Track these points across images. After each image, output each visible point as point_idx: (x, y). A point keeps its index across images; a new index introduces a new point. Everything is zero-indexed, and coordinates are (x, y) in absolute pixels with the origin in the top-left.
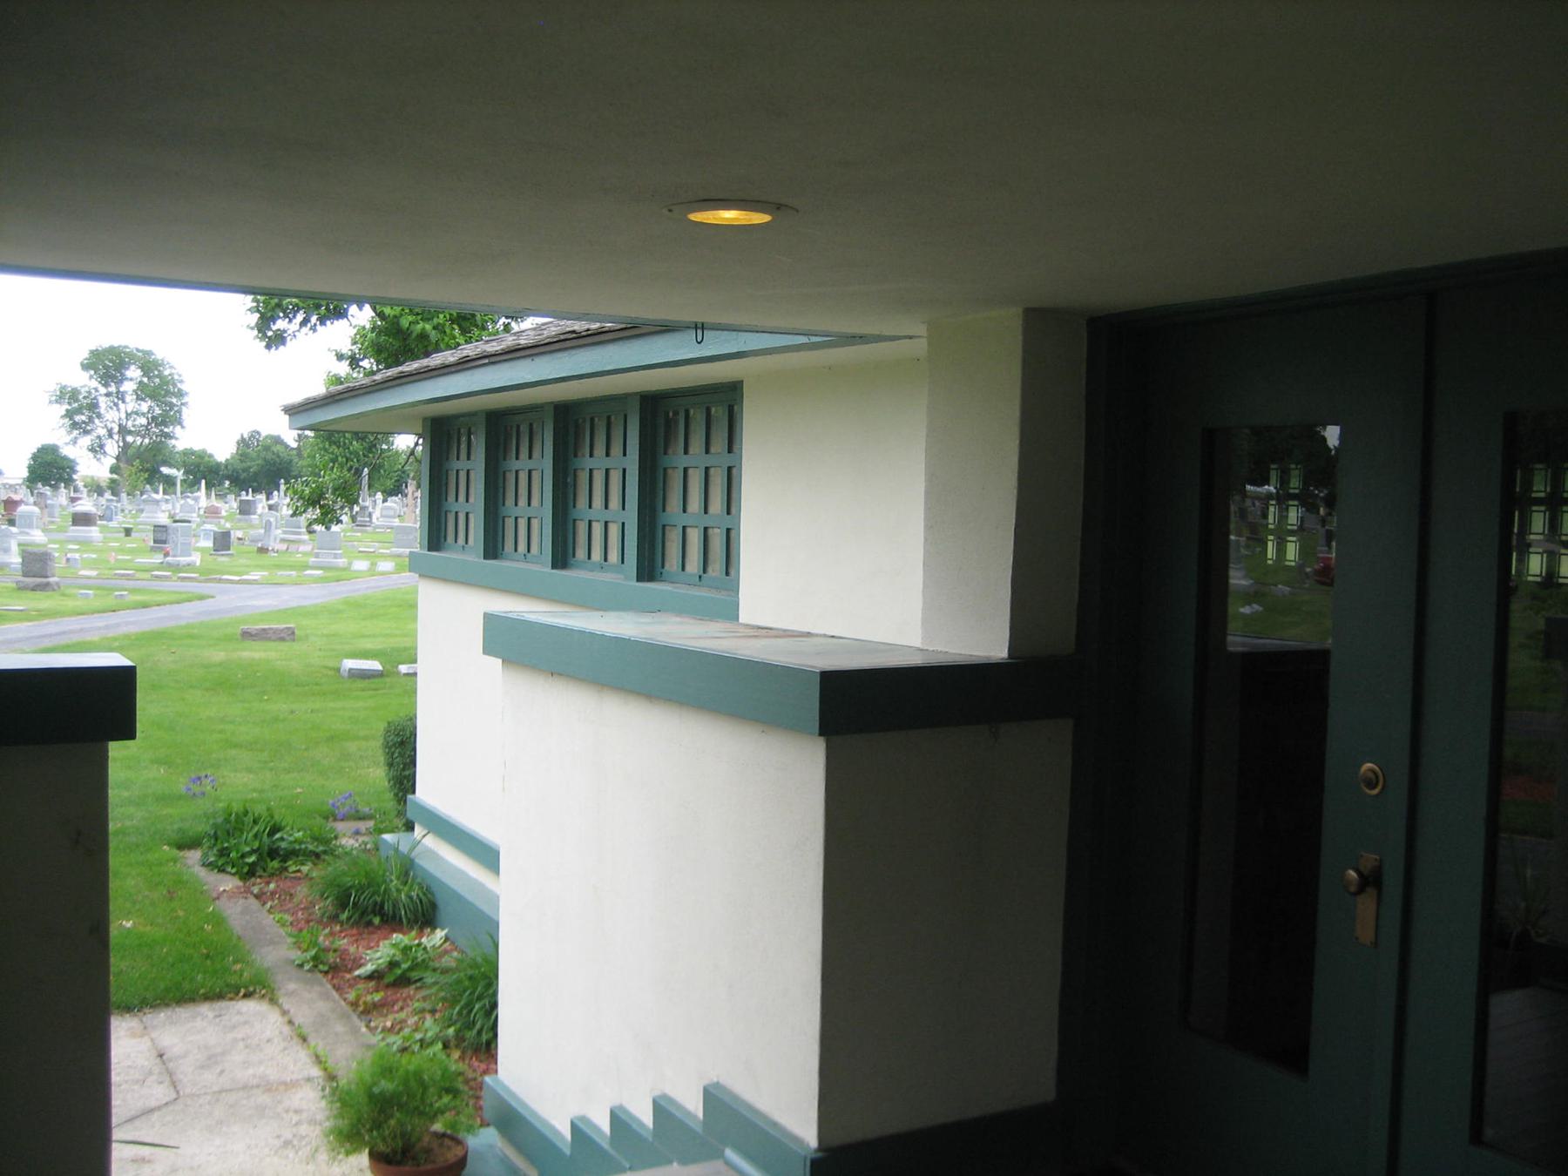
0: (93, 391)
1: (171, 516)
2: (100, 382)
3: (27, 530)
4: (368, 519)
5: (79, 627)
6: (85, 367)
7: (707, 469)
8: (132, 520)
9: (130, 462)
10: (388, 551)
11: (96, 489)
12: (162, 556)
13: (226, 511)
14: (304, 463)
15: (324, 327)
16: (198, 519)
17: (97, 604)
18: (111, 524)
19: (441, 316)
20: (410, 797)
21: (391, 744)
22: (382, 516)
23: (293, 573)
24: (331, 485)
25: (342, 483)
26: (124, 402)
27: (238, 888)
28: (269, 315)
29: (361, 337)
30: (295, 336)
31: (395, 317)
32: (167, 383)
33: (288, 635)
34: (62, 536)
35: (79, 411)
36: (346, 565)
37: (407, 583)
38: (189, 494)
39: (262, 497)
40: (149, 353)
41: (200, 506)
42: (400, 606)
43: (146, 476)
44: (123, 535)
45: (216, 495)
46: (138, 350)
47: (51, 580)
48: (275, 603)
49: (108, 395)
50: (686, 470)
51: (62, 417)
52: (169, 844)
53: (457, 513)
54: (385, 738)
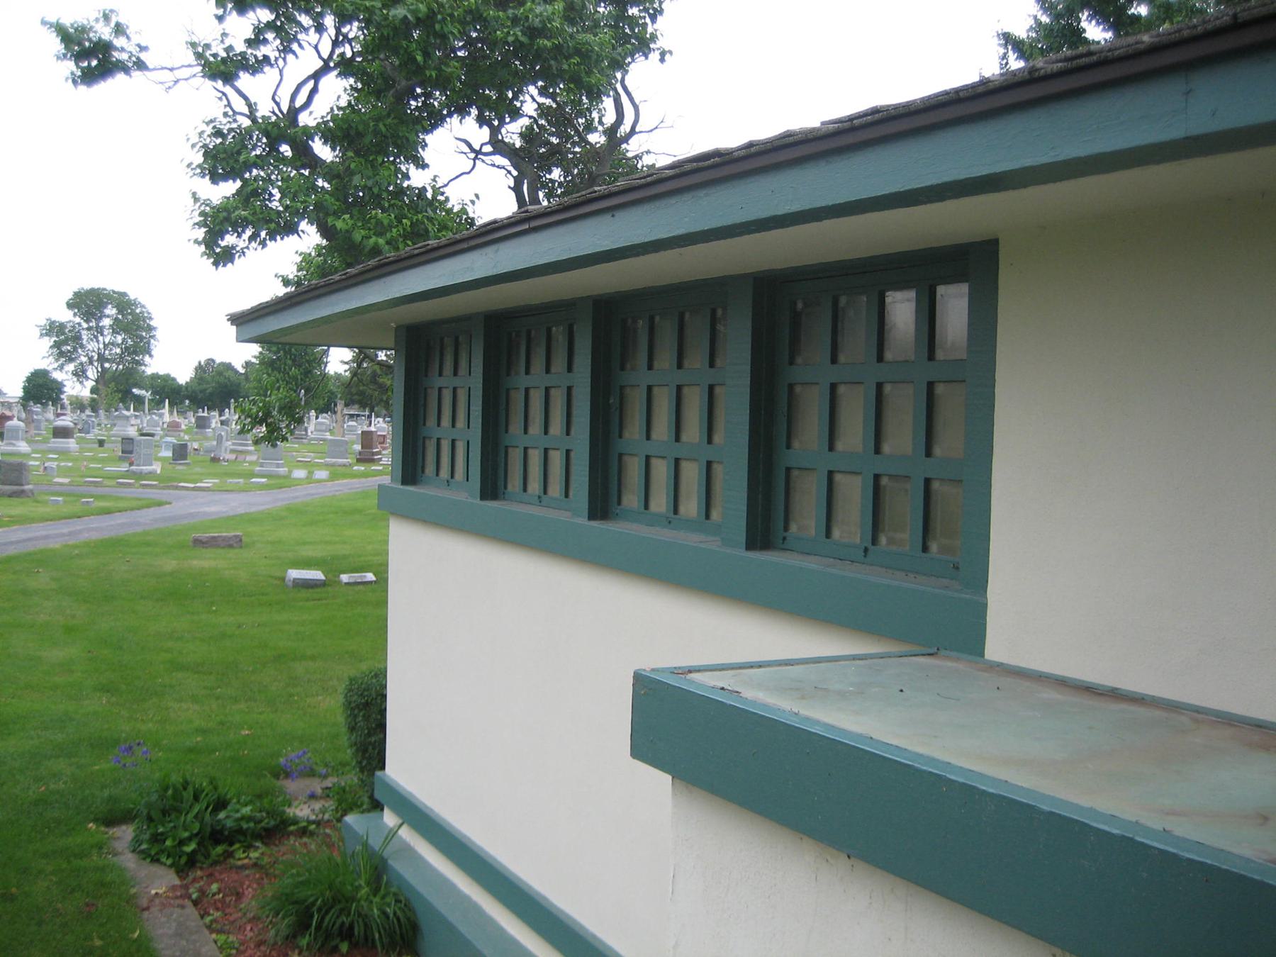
0: (77, 326)
1: (139, 430)
2: (82, 319)
3: (14, 442)
4: (304, 433)
5: (44, 533)
6: (70, 305)
7: (679, 388)
8: (106, 433)
9: (106, 384)
10: (322, 461)
11: (79, 405)
12: (128, 465)
13: (186, 425)
14: (252, 385)
15: (273, 242)
16: (162, 432)
17: (66, 510)
18: (88, 436)
19: (394, 230)
20: (379, 773)
21: (353, 705)
22: (315, 430)
23: (241, 480)
24: (277, 404)
25: (288, 402)
26: (102, 335)
27: (174, 888)
28: (217, 228)
29: (307, 263)
30: (244, 253)
31: (347, 231)
32: (138, 319)
33: (235, 543)
34: (44, 447)
35: (65, 342)
36: (287, 473)
37: (340, 490)
38: (156, 411)
39: (215, 413)
40: (124, 294)
41: (165, 420)
42: (337, 513)
43: (120, 396)
44: (96, 445)
45: (177, 412)
46: (114, 292)
47: (26, 487)
48: (224, 510)
49: (89, 329)
50: (650, 388)
51: (51, 347)
52: (95, 820)
53: (439, 439)
54: (346, 696)
